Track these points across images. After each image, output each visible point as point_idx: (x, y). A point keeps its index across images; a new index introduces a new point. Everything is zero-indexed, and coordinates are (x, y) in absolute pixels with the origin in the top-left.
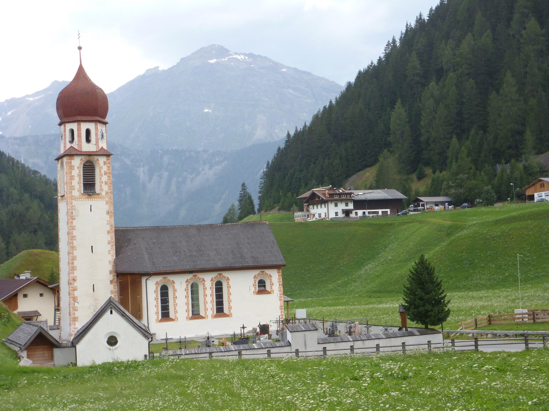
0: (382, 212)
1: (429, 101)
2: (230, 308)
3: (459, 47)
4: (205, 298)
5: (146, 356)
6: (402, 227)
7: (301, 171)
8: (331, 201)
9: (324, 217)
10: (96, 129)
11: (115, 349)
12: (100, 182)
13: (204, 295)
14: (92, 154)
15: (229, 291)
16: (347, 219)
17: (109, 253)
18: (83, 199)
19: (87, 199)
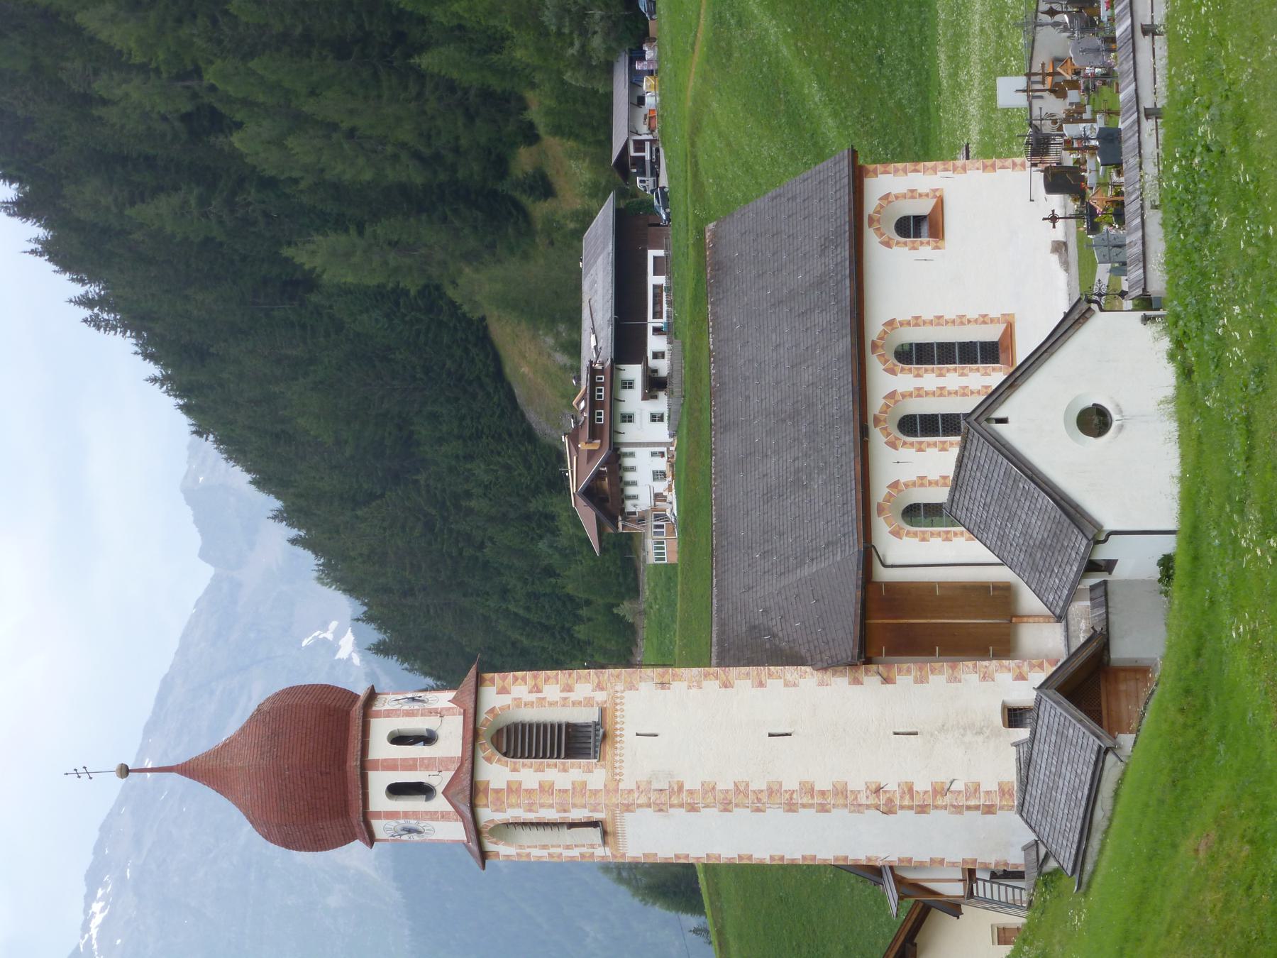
0: (655, 273)
1: (293, 152)
2: (984, 320)
3: (120, 52)
4: (950, 393)
5: (1146, 319)
6: (710, 191)
7: (505, 592)
8: (614, 432)
9: (666, 458)
10: (388, 714)
11: (1120, 412)
12: (564, 706)
13: (941, 395)
14: (471, 726)
15: (931, 323)
16: (675, 385)
17: (795, 685)
18: (618, 758)
19: (618, 745)
